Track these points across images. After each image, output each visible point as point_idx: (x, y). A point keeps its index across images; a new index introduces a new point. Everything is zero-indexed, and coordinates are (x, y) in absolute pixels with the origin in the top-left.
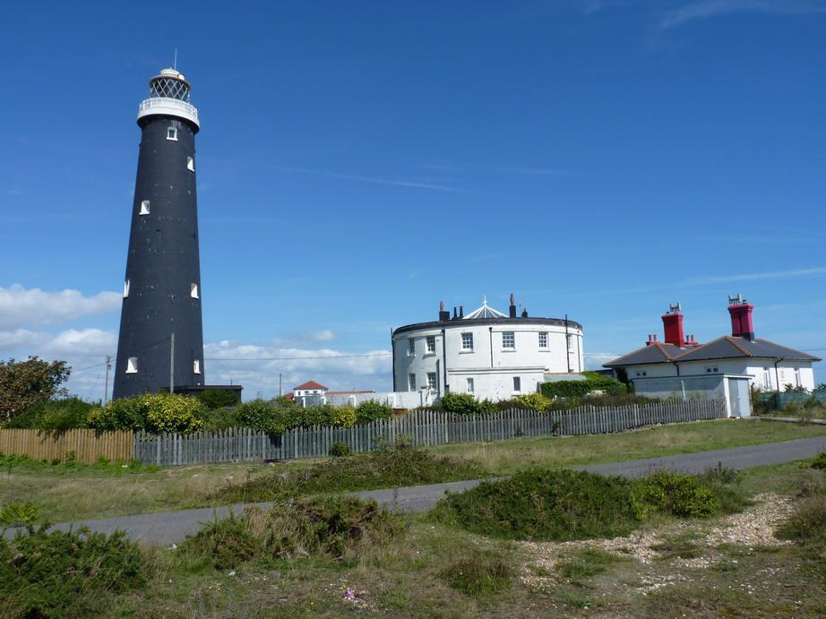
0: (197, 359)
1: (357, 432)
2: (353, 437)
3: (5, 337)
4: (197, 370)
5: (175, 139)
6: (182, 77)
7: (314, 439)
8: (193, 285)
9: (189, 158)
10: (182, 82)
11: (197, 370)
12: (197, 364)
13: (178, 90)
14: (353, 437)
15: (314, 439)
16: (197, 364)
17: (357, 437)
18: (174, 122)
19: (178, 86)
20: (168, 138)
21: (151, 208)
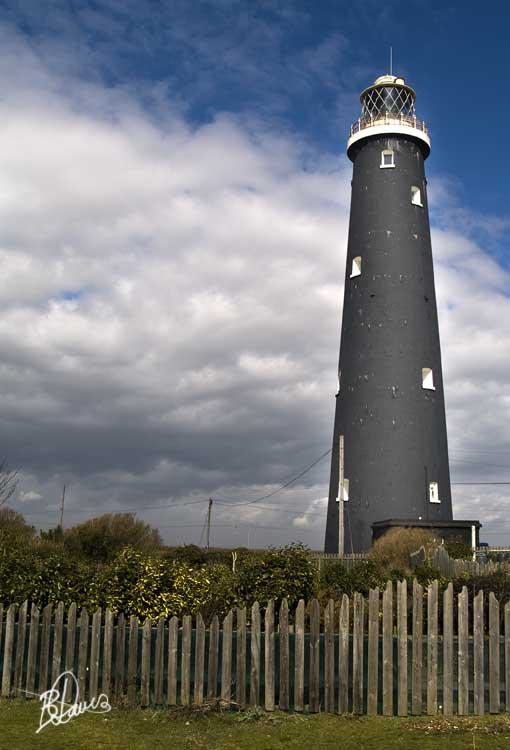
0: (342, 434)
1: (187, 640)
2: (173, 651)
3: (11, 401)
4: (434, 498)
5: (393, 165)
6: (400, 82)
7: (57, 643)
8: (424, 370)
9: (414, 189)
10: (399, 87)
11: (434, 498)
12: (434, 488)
13: (404, 102)
14: (173, 651)
15: (57, 643)
16: (434, 488)
17: (186, 655)
18: (389, 143)
19: (395, 94)
20: (383, 166)
21: (363, 267)
